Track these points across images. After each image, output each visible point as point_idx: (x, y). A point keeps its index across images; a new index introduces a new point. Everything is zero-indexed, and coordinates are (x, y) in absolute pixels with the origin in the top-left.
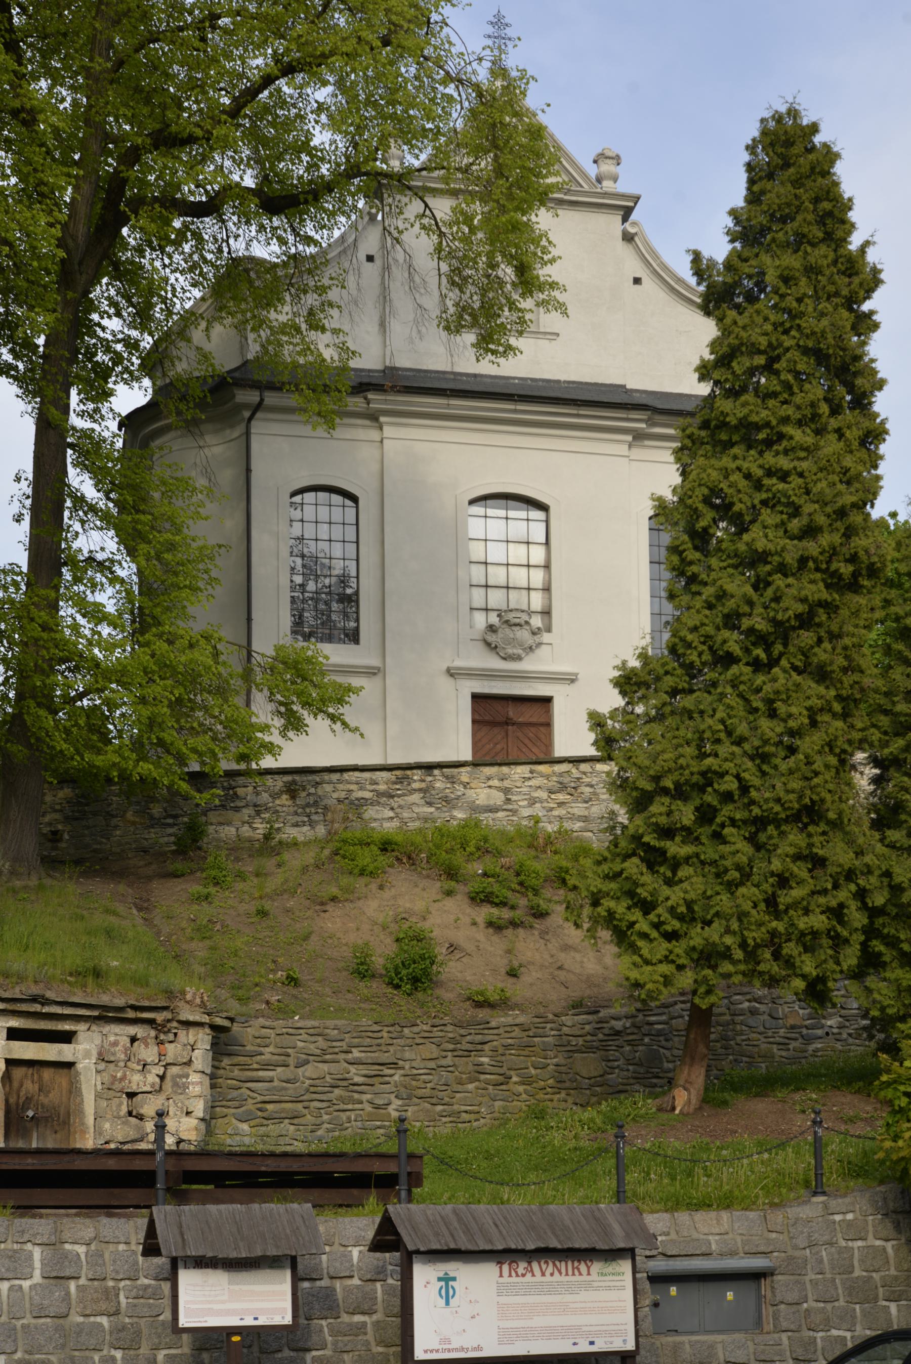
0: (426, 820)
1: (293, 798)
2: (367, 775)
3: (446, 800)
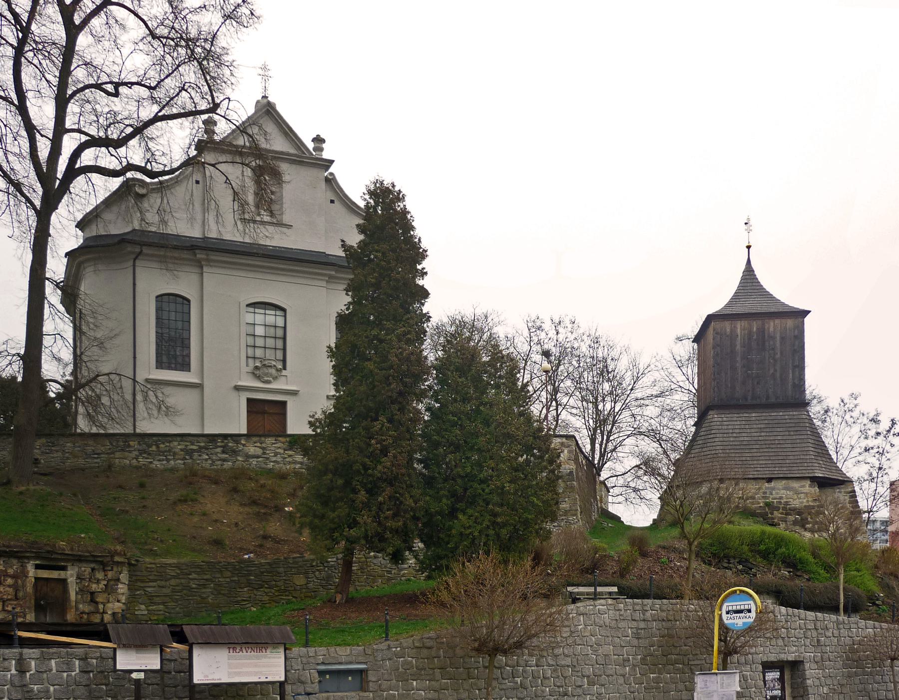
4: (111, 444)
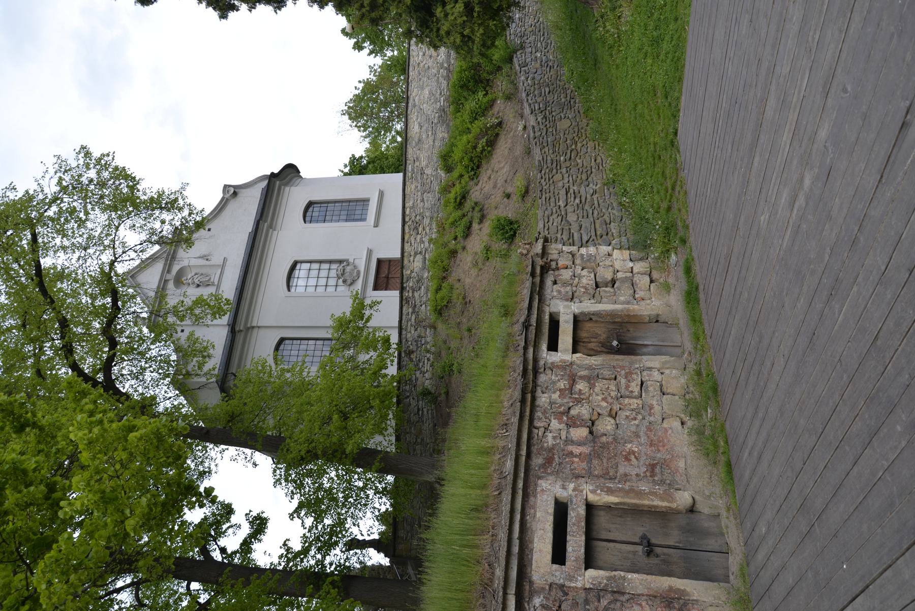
0: (428, 290)
1: (413, 352)
2: (404, 317)
3: (418, 281)
4: (408, 397)
